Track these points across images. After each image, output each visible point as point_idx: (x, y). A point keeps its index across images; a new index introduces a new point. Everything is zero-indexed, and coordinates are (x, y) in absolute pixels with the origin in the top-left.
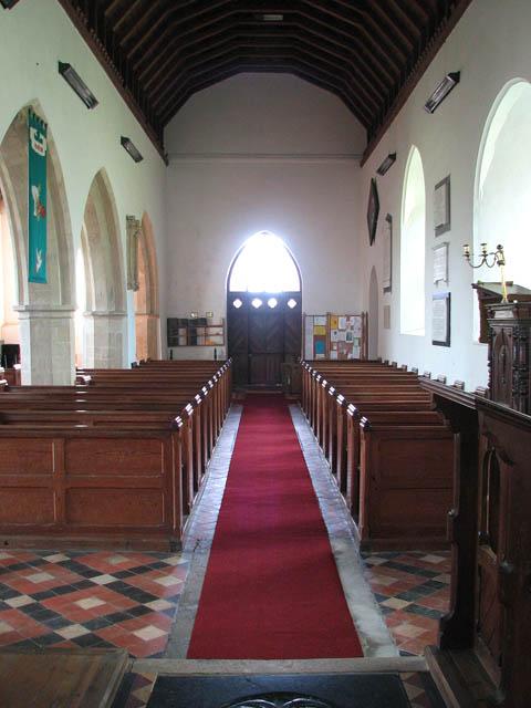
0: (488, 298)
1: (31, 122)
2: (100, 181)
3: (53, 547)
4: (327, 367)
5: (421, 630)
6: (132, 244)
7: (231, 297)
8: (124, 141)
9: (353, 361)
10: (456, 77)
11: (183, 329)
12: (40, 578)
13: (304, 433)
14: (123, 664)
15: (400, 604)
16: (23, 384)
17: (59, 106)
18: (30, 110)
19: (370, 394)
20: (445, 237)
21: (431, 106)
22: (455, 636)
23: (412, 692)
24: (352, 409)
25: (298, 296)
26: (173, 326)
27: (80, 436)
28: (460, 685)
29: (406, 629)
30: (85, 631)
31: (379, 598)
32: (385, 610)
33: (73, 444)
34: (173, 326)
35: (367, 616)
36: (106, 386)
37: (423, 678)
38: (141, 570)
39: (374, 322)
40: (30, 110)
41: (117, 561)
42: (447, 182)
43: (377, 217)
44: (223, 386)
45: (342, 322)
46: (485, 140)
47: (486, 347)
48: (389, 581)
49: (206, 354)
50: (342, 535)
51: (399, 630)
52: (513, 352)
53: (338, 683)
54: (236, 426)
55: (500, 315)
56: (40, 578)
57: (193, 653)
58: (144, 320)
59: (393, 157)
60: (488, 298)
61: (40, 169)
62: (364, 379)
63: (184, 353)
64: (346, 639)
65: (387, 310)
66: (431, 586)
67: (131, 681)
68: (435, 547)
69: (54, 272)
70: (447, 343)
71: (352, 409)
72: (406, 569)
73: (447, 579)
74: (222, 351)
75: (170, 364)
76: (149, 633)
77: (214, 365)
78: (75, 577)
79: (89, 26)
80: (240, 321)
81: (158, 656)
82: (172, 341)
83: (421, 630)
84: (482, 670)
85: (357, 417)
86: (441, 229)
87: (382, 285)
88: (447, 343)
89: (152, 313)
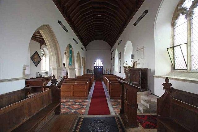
0: (125, 67)
1: (70, 46)
2: (78, 53)
3: (71, 99)
4: (106, 75)
5: (118, 110)
6: (82, 60)
7: (95, 67)
8: (81, 48)
9: (109, 75)
10: (121, 40)
11: (88, 71)
12: (69, 103)
13: (103, 83)
14: (80, 116)
15: (115, 107)
16: (69, 78)
17: (73, 44)
18: (70, 44)
19: (111, 79)
20: (120, 60)
21: (118, 44)
22: (122, 112)
23: (117, 120)
24: (109, 81)
25: (102, 67)
26: (87, 70)
27: (76, 85)
28: (123, 119)
29: (116, 110)
30: (75, 111)
31: (112, 106)
32: (113, 107)
33: (74, 86)
34: (87, 70)
35: (111, 109)
36: (79, 78)
37: (118, 118)
38: (82, 102)
39: (112, 69)
40: (70, 44)
41: (79, 101)
42: (120, 53)
43: (112, 57)
44: (93, 78)
45: (108, 70)
46: (157, 15)
47: (125, 74)
48: (114, 103)
49: (92, 74)
50: (108, 97)
51: (115, 110)
52: (129, 75)
53: (105, 120)
54: (95, 83)
55: (127, 70)
56: (69, 103)
57: (89, 114)
58: (84, 70)
59: (114, 50)
60: (125, 67)
61: (71, 52)
62: (111, 77)
63: (89, 73)
64: (109, 113)
65: (113, 68)
66: (119, 104)
67: (80, 118)
68: (119, 99)
69: (72, 64)
70: (121, 73)
71: (109, 81)
72: (116, 102)
73: (120, 103)
74: (93, 73)
75: (87, 75)
76: (83, 111)
77: (93, 75)
78: (74, 103)
79: (77, 34)
80: (96, 69)
81: (84, 114)
82: (87, 72)
83: (118, 110)
84: (126, 117)
85: (109, 82)
86: (120, 59)
87: (113, 65)
88: (121, 73)
89: (85, 69)
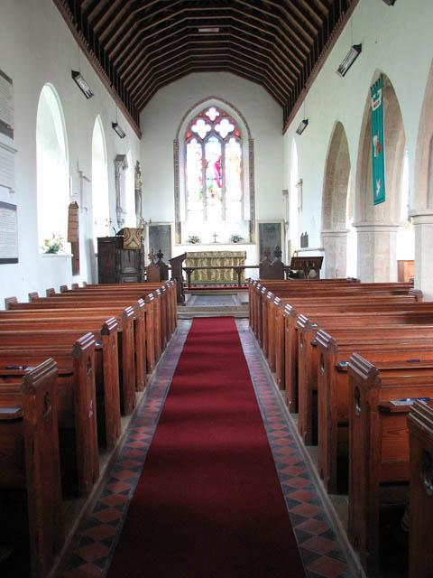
10: (358, 48)
21: (342, 71)
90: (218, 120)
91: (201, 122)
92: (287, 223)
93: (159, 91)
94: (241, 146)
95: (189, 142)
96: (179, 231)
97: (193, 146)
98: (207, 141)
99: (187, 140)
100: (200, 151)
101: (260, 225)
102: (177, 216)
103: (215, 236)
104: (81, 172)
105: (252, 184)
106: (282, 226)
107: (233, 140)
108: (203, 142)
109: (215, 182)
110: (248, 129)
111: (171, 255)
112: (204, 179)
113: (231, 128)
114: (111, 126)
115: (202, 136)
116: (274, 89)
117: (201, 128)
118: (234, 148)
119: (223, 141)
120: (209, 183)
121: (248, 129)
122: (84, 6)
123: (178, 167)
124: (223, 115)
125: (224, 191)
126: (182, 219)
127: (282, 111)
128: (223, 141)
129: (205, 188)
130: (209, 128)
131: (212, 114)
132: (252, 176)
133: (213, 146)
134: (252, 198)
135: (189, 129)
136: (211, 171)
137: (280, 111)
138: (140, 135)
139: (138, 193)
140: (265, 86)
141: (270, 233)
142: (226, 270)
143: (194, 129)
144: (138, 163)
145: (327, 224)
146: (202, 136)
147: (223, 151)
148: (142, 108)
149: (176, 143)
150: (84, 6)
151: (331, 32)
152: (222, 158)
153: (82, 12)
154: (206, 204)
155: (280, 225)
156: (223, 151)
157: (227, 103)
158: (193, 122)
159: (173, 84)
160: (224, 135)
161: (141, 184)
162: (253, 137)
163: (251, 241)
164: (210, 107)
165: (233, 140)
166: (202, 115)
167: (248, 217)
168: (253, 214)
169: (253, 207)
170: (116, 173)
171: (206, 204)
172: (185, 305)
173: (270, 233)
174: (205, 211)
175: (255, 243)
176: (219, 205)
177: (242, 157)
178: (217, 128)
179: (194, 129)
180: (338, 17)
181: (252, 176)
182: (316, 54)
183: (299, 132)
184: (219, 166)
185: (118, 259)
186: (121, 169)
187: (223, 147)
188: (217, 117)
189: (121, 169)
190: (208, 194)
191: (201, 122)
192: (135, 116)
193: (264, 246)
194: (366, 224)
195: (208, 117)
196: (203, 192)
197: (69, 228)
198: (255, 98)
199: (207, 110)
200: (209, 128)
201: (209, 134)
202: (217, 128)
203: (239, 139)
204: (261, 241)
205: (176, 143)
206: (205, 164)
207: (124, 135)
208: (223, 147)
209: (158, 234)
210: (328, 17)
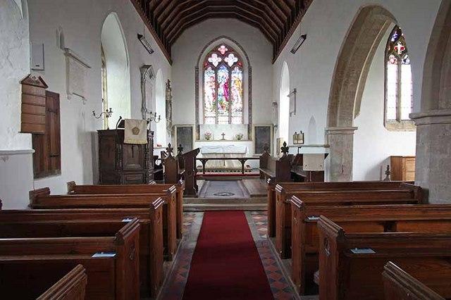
10: (304, 37)
21: (293, 51)
90: (226, 54)
91: (214, 55)
92: (276, 126)
93: (186, 31)
94: (242, 73)
95: (206, 69)
96: (198, 131)
97: (209, 76)
98: (219, 69)
99: (205, 68)
100: (214, 75)
101: (255, 127)
102: (197, 121)
103: (223, 135)
104: (67, 49)
105: (250, 99)
106: (271, 129)
107: (237, 69)
108: (216, 69)
109: (224, 98)
110: (248, 60)
111: (192, 148)
112: (216, 95)
113: (236, 60)
114: (136, 36)
115: (216, 65)
116: (267, 29)
117: (215, 60)
118: (237, 75)
119: (230, 69)
120: (220, 98)
121: (248, 60)
122: (151, 4)
123: (198, 86)
124: (230, 50)
125: (230, 103)
126: (201, 123)
127: (272, 47)
128: (230, 69)
129: (217, 101)
130: (220, 60)
131: (223, 49)
132: (250, 93)
133: (223, 73)
134: (250, 109)
135: (206, 60)
136: (221, 90)
137: (271, 47)
138: (171, 62)
139: (168, 103)
140: (261, 29)
141: (262, 135)
142: (266, 205)
143: (210, 60)
144: (169, 81)
145: (332, 123)
146: (216, 65)
147: (230, 76)
148: (174, 40)
149: (197, 68)
150: (151, 4)
151: (297, 15)
152: (229, 80)
153: (150, 8)
154: (217, 113)
155: (270, 127)
156: (230, 76)
157: (233, 41)
158: (209, 55)
159: (196, 26)
160: (230, 64)
161: (171, 97)
162: (251, 65)
163: (249, 139)
164: (221, 45)
165: (237, 69)
166: (216, 50)
167: (247, 122)
168: (250, 120)
169: (250, 115)
170: (142, 78)
171: (217, 113)
172: (197, 197)
173: (262, 135)
174: (216, 117)
175: (251, 140)
176: (226, 113)
177: (243, 80)
178: (226, 60)
179: (210, 60)
180: (298, 12)
181: (250, 93)
182: (285, 32)
183: (293, 51)
184: (228, 86)
185: (119, 155)
186: (147, 76)
187: (230, 74)
188: (226, 52)
189: (147, 76)
190: (219, 105)
191: (214, 55)
192: (167, 46)
193: (259, 142)
194: (439, 113)
195: (220, 52)
196: (215, 104)
197: (23, 113)
198: (254, 38)
199: (219, 46)
200: (220, 60)
201: (220, 63)
202: (226, 60)
203: (241, 68)
204: (256, 139)
205: (197, 68)
206: (217, 86)
207: (153, 52)
208: (230, 74)
209: (183, 133)
210: (290, 14)
